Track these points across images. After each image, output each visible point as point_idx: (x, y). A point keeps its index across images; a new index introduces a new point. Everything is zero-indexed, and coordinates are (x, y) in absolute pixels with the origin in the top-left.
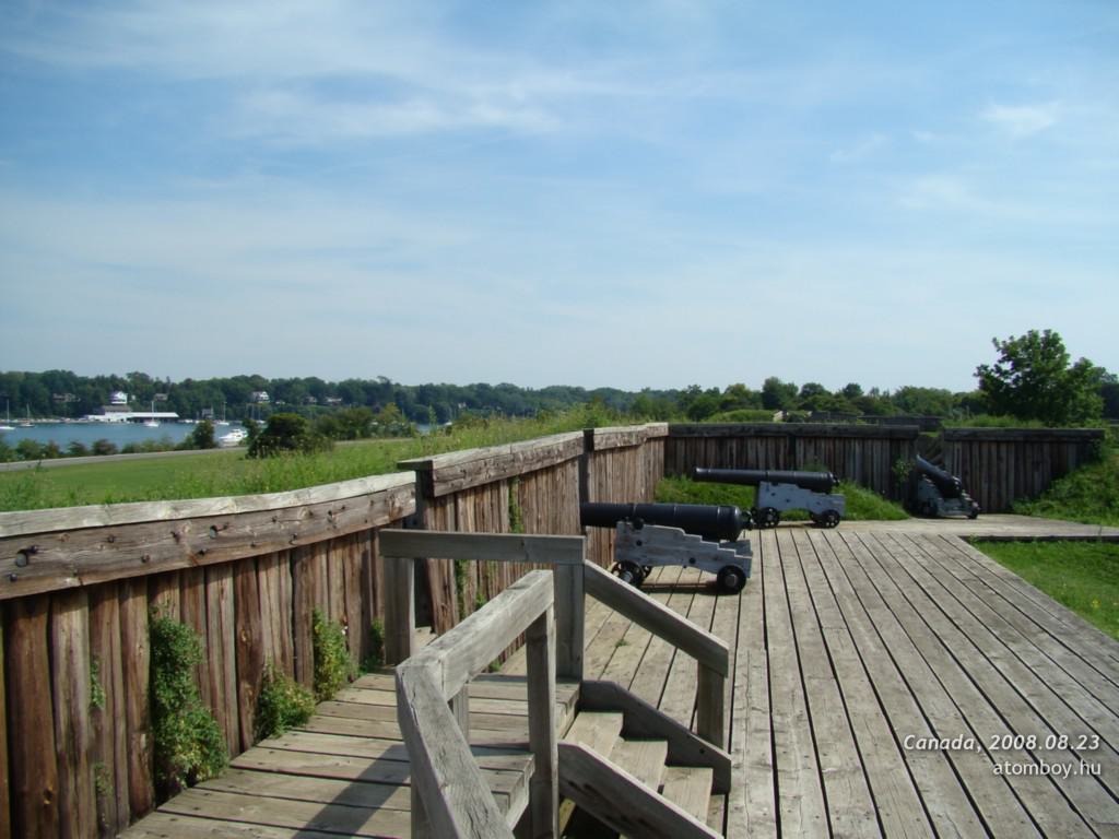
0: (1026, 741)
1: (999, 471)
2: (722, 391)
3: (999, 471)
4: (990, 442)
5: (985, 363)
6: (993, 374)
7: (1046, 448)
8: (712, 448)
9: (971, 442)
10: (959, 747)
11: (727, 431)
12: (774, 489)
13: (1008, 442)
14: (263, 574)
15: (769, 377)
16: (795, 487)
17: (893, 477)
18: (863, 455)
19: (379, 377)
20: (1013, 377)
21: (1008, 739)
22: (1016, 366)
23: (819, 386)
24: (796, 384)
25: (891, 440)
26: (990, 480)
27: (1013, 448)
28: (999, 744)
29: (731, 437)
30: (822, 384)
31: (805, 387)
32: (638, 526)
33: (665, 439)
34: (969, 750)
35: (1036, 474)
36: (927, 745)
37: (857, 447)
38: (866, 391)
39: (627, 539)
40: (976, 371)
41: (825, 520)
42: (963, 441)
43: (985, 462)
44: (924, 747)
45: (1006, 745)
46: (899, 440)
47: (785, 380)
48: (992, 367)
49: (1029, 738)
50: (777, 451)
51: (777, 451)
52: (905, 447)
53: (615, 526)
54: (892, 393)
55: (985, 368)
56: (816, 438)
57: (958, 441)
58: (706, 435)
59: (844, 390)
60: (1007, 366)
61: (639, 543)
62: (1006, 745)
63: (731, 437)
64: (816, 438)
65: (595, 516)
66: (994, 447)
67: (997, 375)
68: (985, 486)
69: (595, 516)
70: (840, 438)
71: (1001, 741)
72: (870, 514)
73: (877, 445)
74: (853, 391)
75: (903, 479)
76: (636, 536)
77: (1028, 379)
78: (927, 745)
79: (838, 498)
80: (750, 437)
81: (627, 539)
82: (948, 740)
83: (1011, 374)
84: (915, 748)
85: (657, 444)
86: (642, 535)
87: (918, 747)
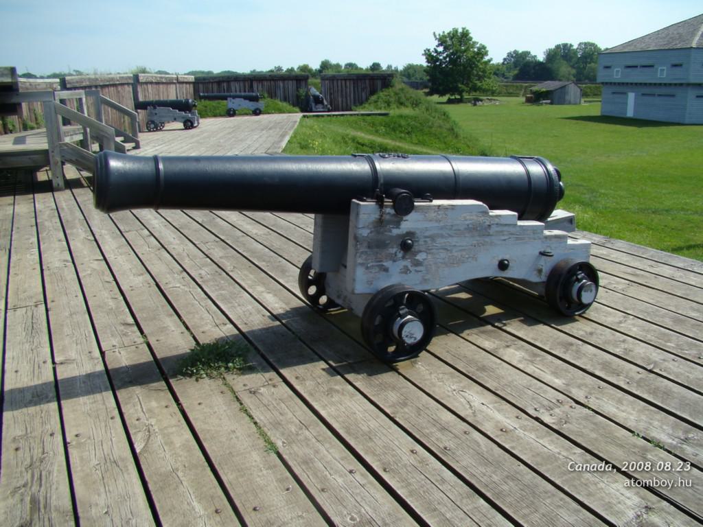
0: (645, 465)
1: (346, 93)
2: (296, 69)
3: (346, 93)
4: (341, 80)
5: (429, 48)
6: (433, 54)
7: (367, 82)
8: (215, 87)
9: (333, 80)
10: (603, 469)
11: (221, 79)
12: (232, 100)
13: (350, 80)
14: (374, 203)
15: (377, 61)
16: (242, 99)
17: (298, 97)
18: (284, 88)
19: (74, 71)
20: (445, 55)
21: (633, 464)
22: (446, 49)
23: (355, 64)
24: (341, 64)
25: (297, 80)
26: (342, 97)
27: (352, 82)
28: (628, 468)
29: (224, 81)
30: (356, 63)
31: (346, 65)
32: (155, 108)
33: (193, 83)
34: (579, 471)
35: (363, 94)
36: (582, 468)
37: (281, 84)
38: (384, 67)
39: (151, 113)
40: (424, 52)
41: (257, 112)
42: (330, 80)
43: (340, 88)
44: (595, 469)
45: (632, 468)
46: (300, 80)
47: (333, 61)
48: (432, 49)
49: (646, 464)
50: (245, 87)
51: (245, 87)
52: (303, 83)
53: (146, 109)
54: (401, 68)
55: (429, 50)
56: (262, 80)
57: (327, 79)
58: (212, 81)
59: (371, 67)
60: (441, 49)
61: (156, 114)
62: (632, 468)
63: (224, 81)
64: (262, 80)
65: (140, 106)
66: (343, 82)
67: (435, 55)
68: (340, 99)
69: (140, 106)
70: (273, 80)
71: (629, 465)
72: (281, 111)
73: (290, 82)
74: (376, 67)
75: (303, 97)
76: (154, 112)
77: (596, 53)
78: (582, 468)
79: (261, 104)
80: (232, 81)
81: (151, 113)
82: (596, 465)
83: (443, 53)
84: (575, 470)
85: (188, 85)
86: (156, 111)
87: (577, 469)
